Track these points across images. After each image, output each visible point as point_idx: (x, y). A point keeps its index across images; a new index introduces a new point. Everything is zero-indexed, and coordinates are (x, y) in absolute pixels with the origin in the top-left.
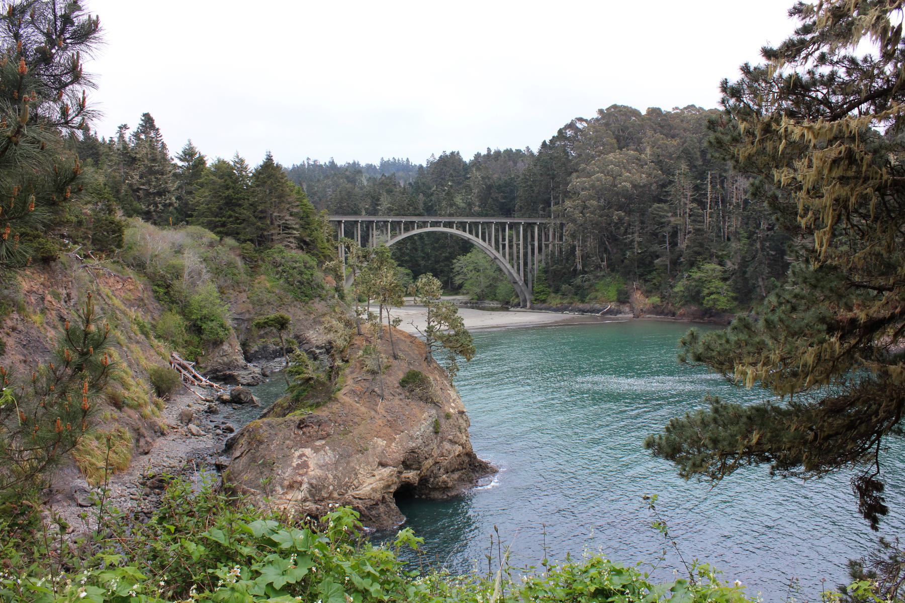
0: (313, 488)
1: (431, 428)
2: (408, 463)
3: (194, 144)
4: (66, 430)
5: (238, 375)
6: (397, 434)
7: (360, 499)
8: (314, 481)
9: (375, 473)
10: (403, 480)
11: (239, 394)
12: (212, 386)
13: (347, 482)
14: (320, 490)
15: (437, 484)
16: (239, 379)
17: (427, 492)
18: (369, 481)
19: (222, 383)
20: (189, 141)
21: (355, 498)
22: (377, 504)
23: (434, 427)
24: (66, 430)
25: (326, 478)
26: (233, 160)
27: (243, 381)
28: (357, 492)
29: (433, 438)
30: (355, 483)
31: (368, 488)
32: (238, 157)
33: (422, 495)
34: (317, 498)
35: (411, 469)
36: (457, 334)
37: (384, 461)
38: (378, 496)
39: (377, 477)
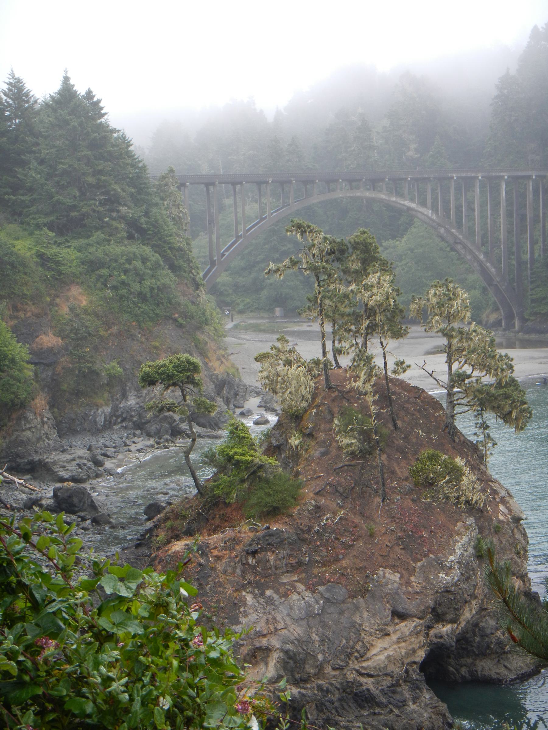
0: (290, 658)
1: (470, 549)
2: (439, 611)
3: (92, 89)
4: (377, 582)
5: (54, 463)
6: (416, 560)
7: (369, 676)
8: (290, 647)
9: (390, 629)
10: (435, 640)
11: (70, 497)
12: (12, 482)
13: (344, 648)
14: (304, 661)
15: (488, 647)
16: (56, 469)
17: (470, 661)
18: (380, 644)
19: (28, 476)
20: (66, 79)
21: (361, 674)
22: (398, 685)
23: (475, 548)
24: (377, 582)
25: (310, 641)
26: (7, 81)
27: (65, 474)
28: (365, 664)
29: (475, 566)
30: (358, 647)
31: (382, 657)
32: (13, 75)
33: (462, 666)
34: (297, 676)
35: (443, 621)
36: (499, 385)
37: (400, 609)
38: (397, 670)
39: (394, 637)
